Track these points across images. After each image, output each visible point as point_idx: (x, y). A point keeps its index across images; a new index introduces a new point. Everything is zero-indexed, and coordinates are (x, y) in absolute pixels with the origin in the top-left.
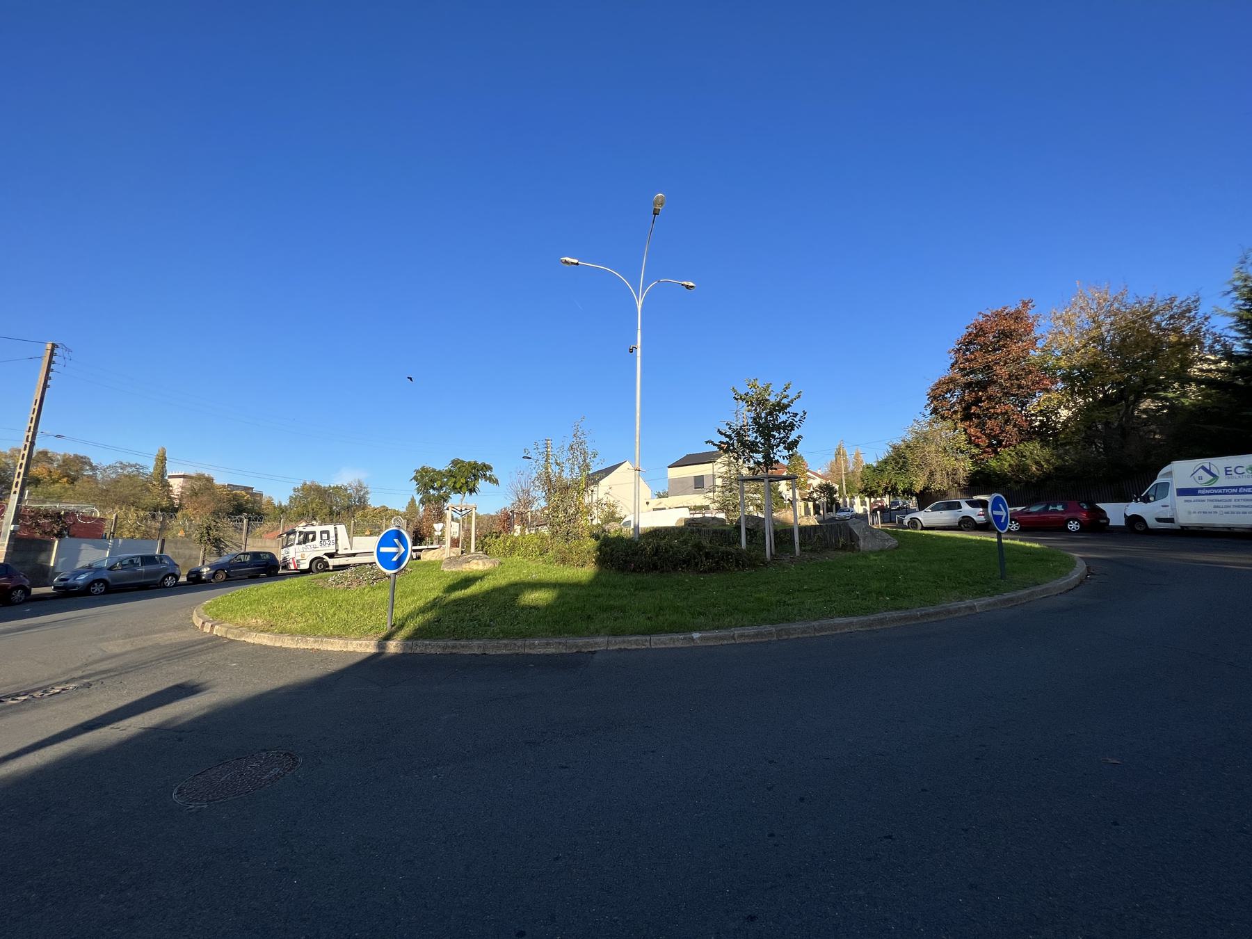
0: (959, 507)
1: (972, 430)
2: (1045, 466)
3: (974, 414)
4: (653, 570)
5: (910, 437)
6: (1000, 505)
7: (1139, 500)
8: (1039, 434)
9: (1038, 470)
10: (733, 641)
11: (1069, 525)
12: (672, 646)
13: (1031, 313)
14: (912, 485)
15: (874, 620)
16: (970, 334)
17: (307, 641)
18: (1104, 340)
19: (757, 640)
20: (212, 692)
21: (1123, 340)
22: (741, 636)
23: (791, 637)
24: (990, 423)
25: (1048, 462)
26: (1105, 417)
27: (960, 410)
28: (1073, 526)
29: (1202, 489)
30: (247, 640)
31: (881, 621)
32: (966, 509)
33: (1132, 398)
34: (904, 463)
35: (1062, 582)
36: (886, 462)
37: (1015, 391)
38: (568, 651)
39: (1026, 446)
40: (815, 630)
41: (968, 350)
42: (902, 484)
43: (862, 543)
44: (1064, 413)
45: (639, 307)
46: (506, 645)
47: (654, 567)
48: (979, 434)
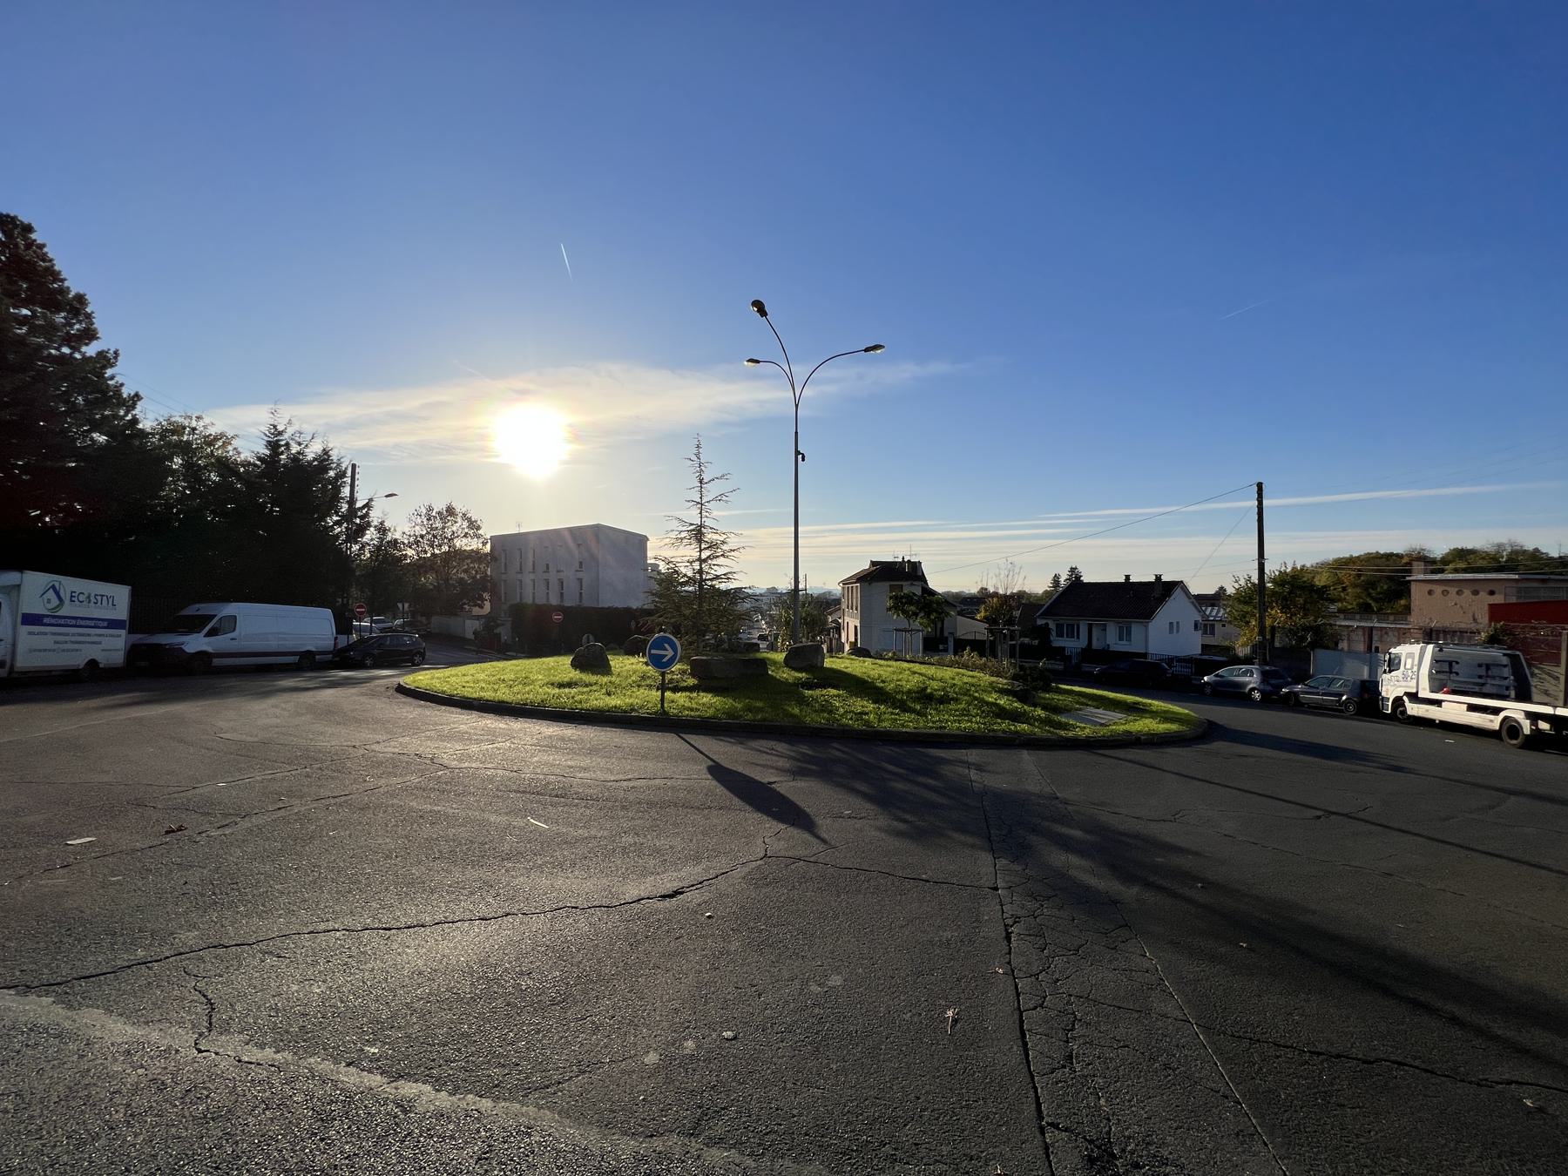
20: (1162, 752)
29: (48, 616)
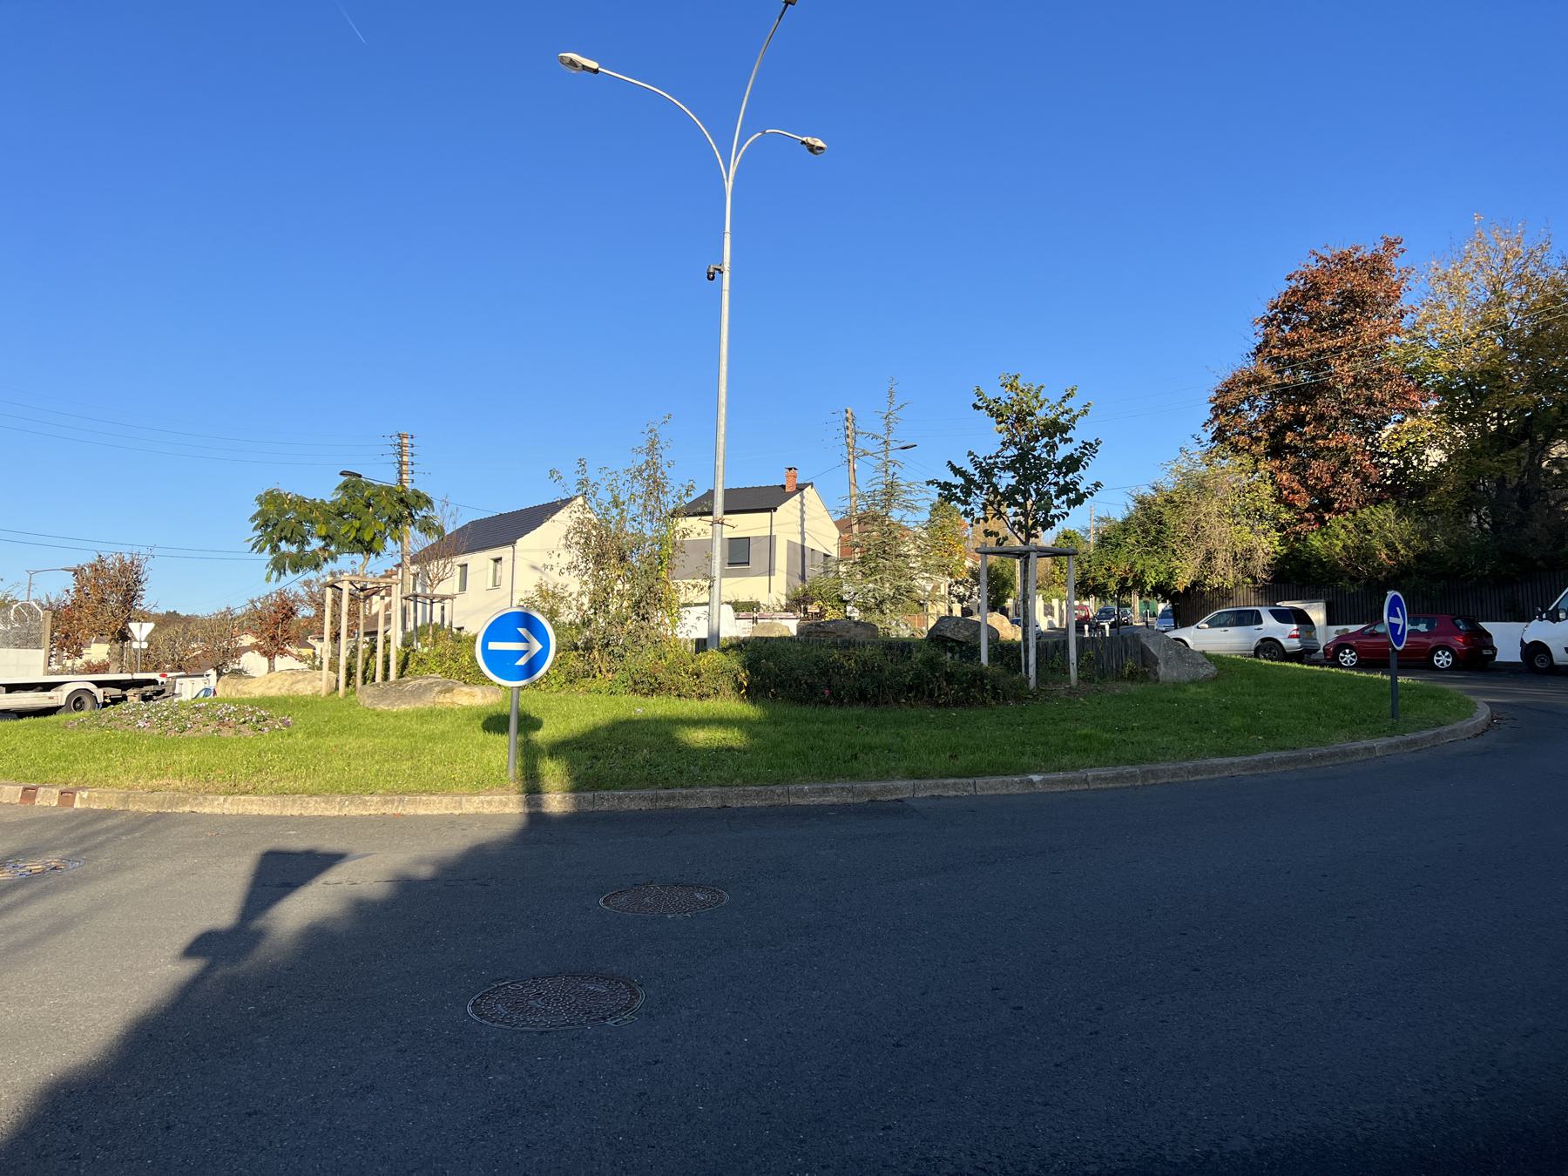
0: (1259, 621)
1: (1285, 478)
2: (1402, 552)
3: (1288, 446)
4: (859, 700)
5: (1169, 482)
6: (1398, 609)
7: (1544, 616)
8: (1395, 491)
9: (1389, 558)
10: (1086, 787)
11: (1436, 658)
12: (1005, 792)
13: (1398, 263)
14: (1171, 575)
15: (1259, 761)
16: (1294, 292)
17: (365, 803)
18: (1507, 328)
19: (1118, 785)
21: (1536, 332)
22: (1097, 778)
23: (1160, 782)
24: (1316, 466)
25: (1407, 544)
26: (1501, 469)
27: (1266, 436)
28: (1443, 659)
30: (198, 810)
31: (1267, 763)
32: (1270, 626)
33: (1541, 437)
34: (1159, 532)
35: (1469, 723)
36: (1125, 527)
37: (1361, 409)
38: (856, 800)
39: (1372, 513)
40: (1189, 772)
41: (1286, 321)
42: (1154, 574)
43: (1162, 670)
44: (1435, 456)
45: (729, 186)
46: (758, 793)
47: (862, 697)
48: (1295, 485)
